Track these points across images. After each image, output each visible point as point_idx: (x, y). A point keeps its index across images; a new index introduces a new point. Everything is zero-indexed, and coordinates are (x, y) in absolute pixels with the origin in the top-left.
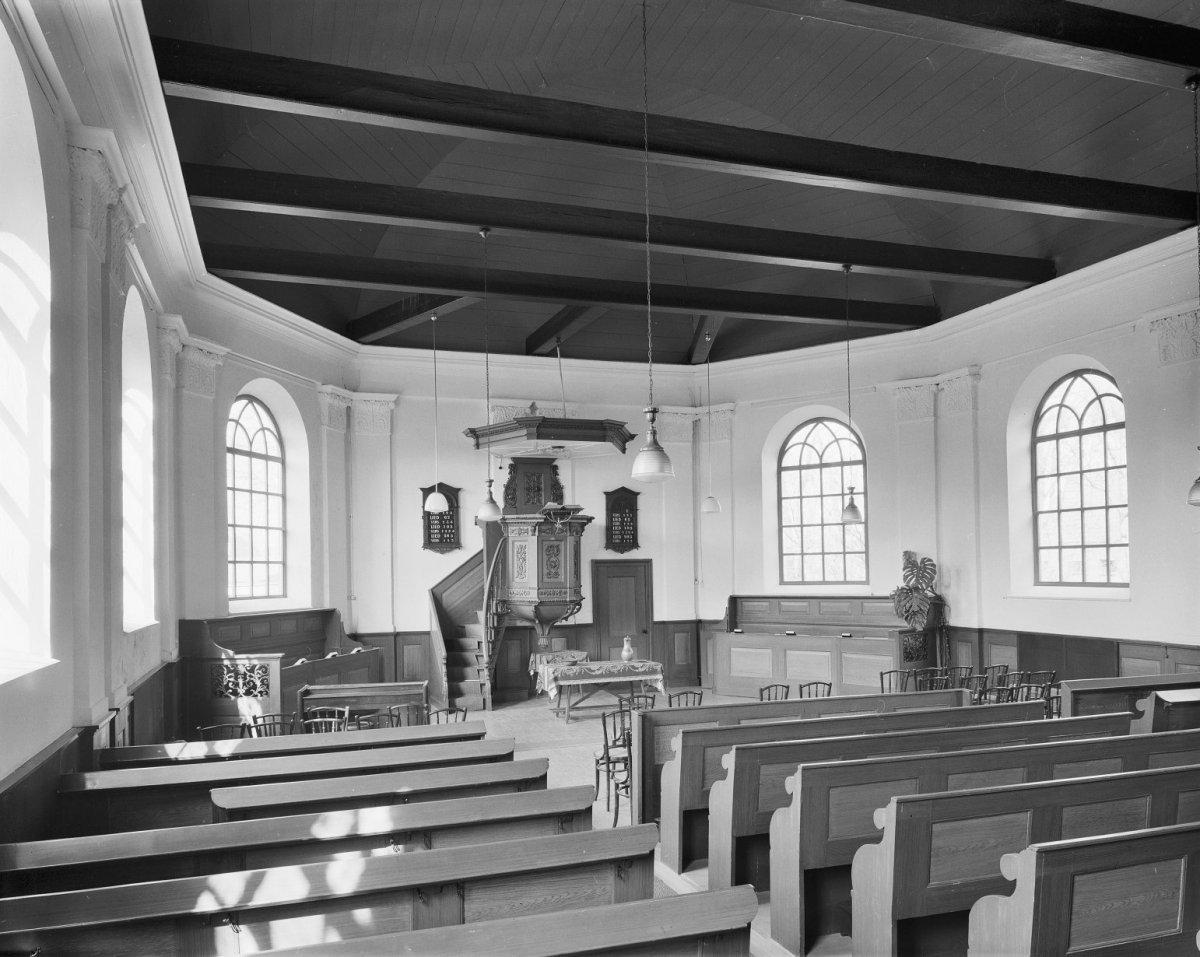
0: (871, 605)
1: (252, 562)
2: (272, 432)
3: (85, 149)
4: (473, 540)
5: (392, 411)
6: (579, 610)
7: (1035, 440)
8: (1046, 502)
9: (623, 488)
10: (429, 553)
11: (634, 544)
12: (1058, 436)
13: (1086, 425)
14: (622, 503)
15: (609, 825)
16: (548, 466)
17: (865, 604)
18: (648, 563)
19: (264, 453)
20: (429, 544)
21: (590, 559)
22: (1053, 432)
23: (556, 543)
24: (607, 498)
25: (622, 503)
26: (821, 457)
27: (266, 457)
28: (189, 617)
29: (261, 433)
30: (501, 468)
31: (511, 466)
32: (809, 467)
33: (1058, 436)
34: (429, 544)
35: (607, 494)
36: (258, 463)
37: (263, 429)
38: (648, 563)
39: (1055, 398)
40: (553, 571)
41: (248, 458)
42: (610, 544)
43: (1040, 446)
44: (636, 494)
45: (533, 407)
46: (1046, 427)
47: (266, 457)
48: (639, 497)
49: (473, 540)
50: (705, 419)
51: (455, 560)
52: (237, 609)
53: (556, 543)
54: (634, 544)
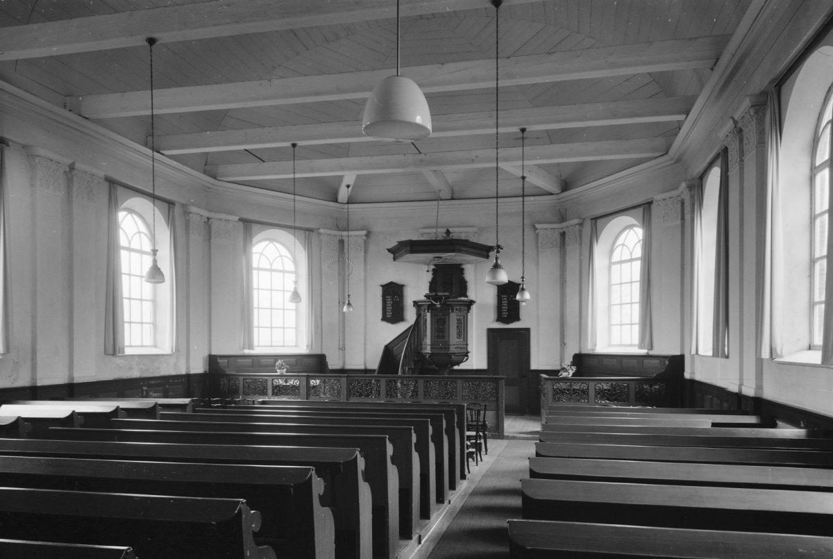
1: (621, 325)
2: (146, 235)
3: (712, 69)
4: (411, 315)
5: (240, 220)
6: (467, 360)
7: (611, 264)
10: (384, 323)
11: (517, 318)
12: (621, 262)
13: (634, 257)
14: (508, 295)
16: (458, 270)
18: (528, 330)
20: (384, 319)
22: (618, 259)
24: (383, 289)
25: (508, 295)
29: (138, 235)
30: (428, 271)
31: (434, 270)
33: (621, 262)
34: (384, 319)
35: (382, 286)
36: (135, 256)
37: (139, 232)
38: (528, 330)
39: (620, 241)
40: (441, 334)
42: (500, 318)
43: (614, 267)
45: (448, 232)
46: (616, 257)
47: (142, 252)
49: (411, 315)
50: (346, 239)
53: (443, 317)
54: (517, 318)
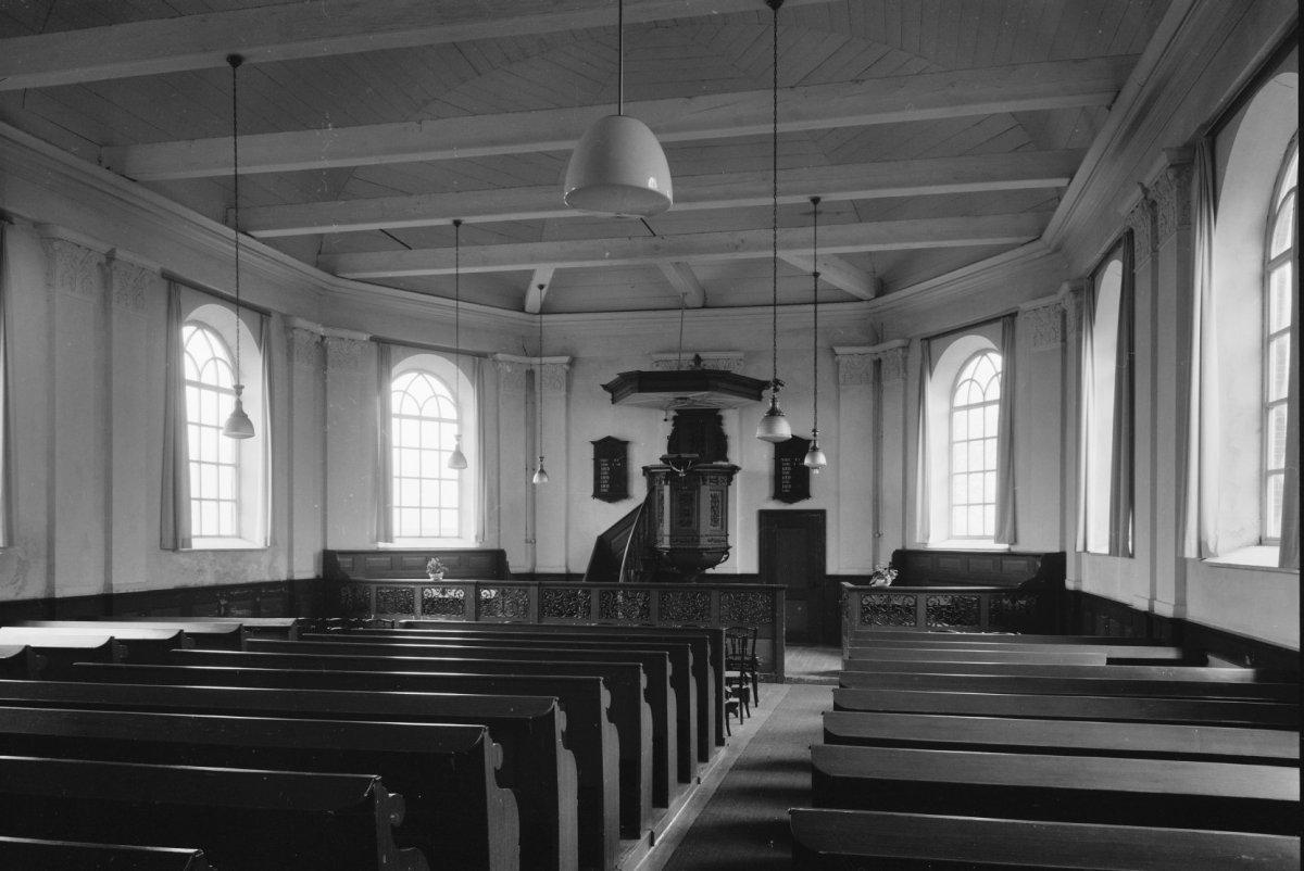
0: (1010, 562)
2: (226, 362)
4: (639, 490)
6: (727, 559)
8: (960, 465)
9: (609, 438)
11: (807, 495)
12: (968, 407)
15: (1294, 774)
16: (713, 418)
17: (971, 560)
19: (214, 383)
20: (598, 494)
21: (827, 508)
23: (690, 492)
25: (791, 458)
26: (421, 410)
27: (218, 389)
28: (329, 548)
29: (212, 363)
31: (675, 418)
32: (408, 417)
33: (968, 407)
34: (598, 494)
36: (208, 395)
38: (822, 513)
39: (967, 374)
41: (221, 386)
42: (778, 495)
44: (625, 443)
45: (698, 359)
46: (960, 400)
47: (218, 389)
48: (629, 445)
49: (639, 490)
50: (537, 369)
51: (621, 510)
52: (398, 544)
